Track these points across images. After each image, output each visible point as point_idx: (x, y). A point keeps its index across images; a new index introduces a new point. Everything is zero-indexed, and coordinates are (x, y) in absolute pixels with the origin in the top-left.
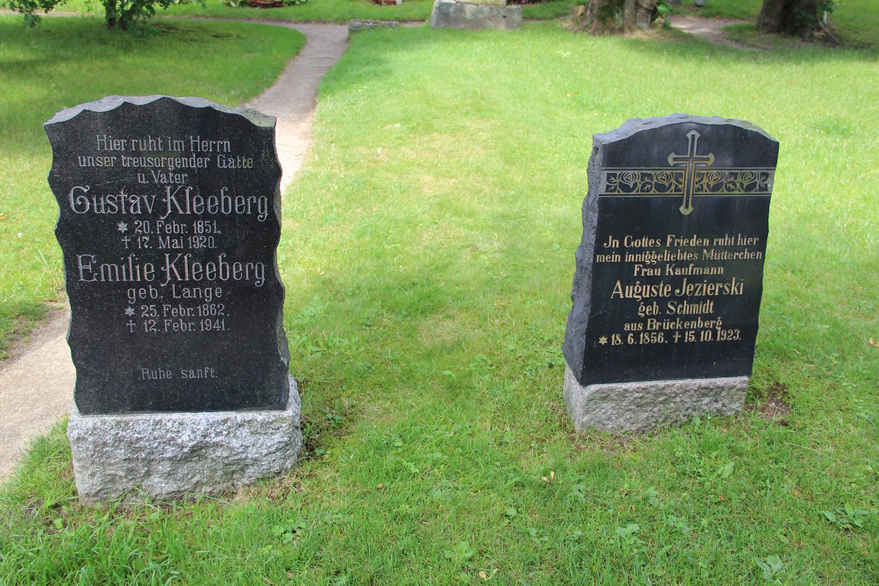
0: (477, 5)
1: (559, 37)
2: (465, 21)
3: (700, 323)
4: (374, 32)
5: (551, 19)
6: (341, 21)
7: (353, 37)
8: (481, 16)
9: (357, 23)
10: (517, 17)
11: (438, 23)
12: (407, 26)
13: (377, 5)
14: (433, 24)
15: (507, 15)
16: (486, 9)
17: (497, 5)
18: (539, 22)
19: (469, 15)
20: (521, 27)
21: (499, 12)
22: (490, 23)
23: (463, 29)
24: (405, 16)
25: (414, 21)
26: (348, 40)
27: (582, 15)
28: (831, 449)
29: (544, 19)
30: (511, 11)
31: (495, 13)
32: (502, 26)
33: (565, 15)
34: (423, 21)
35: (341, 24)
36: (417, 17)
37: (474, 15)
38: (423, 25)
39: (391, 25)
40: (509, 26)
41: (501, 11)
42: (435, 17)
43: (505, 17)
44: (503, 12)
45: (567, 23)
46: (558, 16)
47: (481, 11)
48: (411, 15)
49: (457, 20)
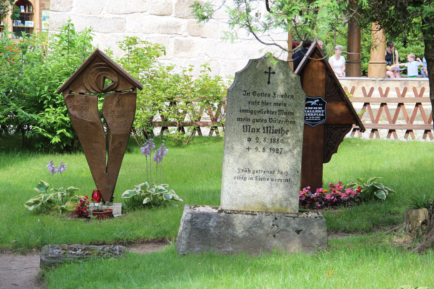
0: (253, 214)
1: (398, 261)
2: (234, 240)
3: (91, 85)
4: (86, 264)
5: (368, 231)
6: (24, 248)
7: (51, 275)
8: (261, 232)
9: (56, 252)
10: (318, 231)
11: (189, 245)
12: (133, 251)
13: (83, 220)
14: (182, 248)
15: (303, 228)
16: (268, 220)
17: (285, 214)
18: (351, 237)
19: (240, 231)
20: (326, 245)
21: (288, 225)
22: (275, 242)
23: (229, 253)
24: (130, 235)
25: (144, 242)
26: (41, 279)
27: (424, 223)
28: (39, 45)
29: (356, 231)
30: (308, 222)
31: (282, 226)
32: (295, 246)
33: (393, 223)
34: (162, 241)
35: (23, 253)
36: (151, 237)
37: (248, 230)
38: (164, 249)
39: (112, 252)
40: (307, 246)
41: (292, 222)
42: (184, 236)
43: (298, 232)
44: (294, 224)
45: (401, 238)
46: (376, 226)
47: (259, 224)
48: (140, 233)
49: (220, 239)
